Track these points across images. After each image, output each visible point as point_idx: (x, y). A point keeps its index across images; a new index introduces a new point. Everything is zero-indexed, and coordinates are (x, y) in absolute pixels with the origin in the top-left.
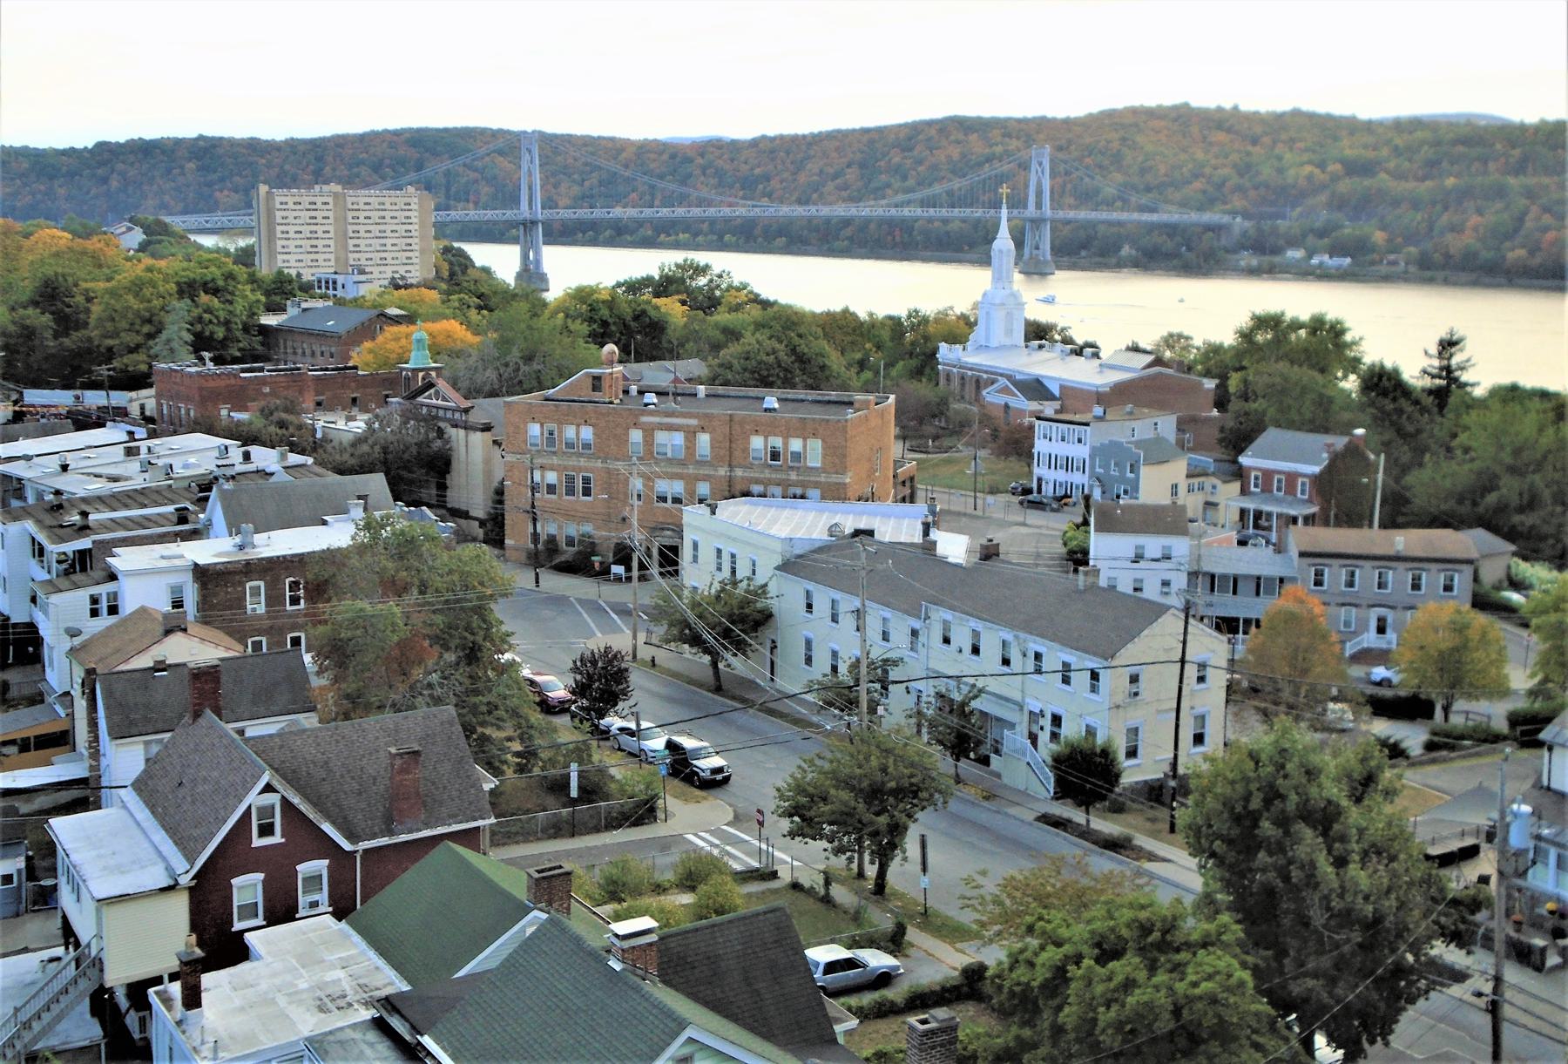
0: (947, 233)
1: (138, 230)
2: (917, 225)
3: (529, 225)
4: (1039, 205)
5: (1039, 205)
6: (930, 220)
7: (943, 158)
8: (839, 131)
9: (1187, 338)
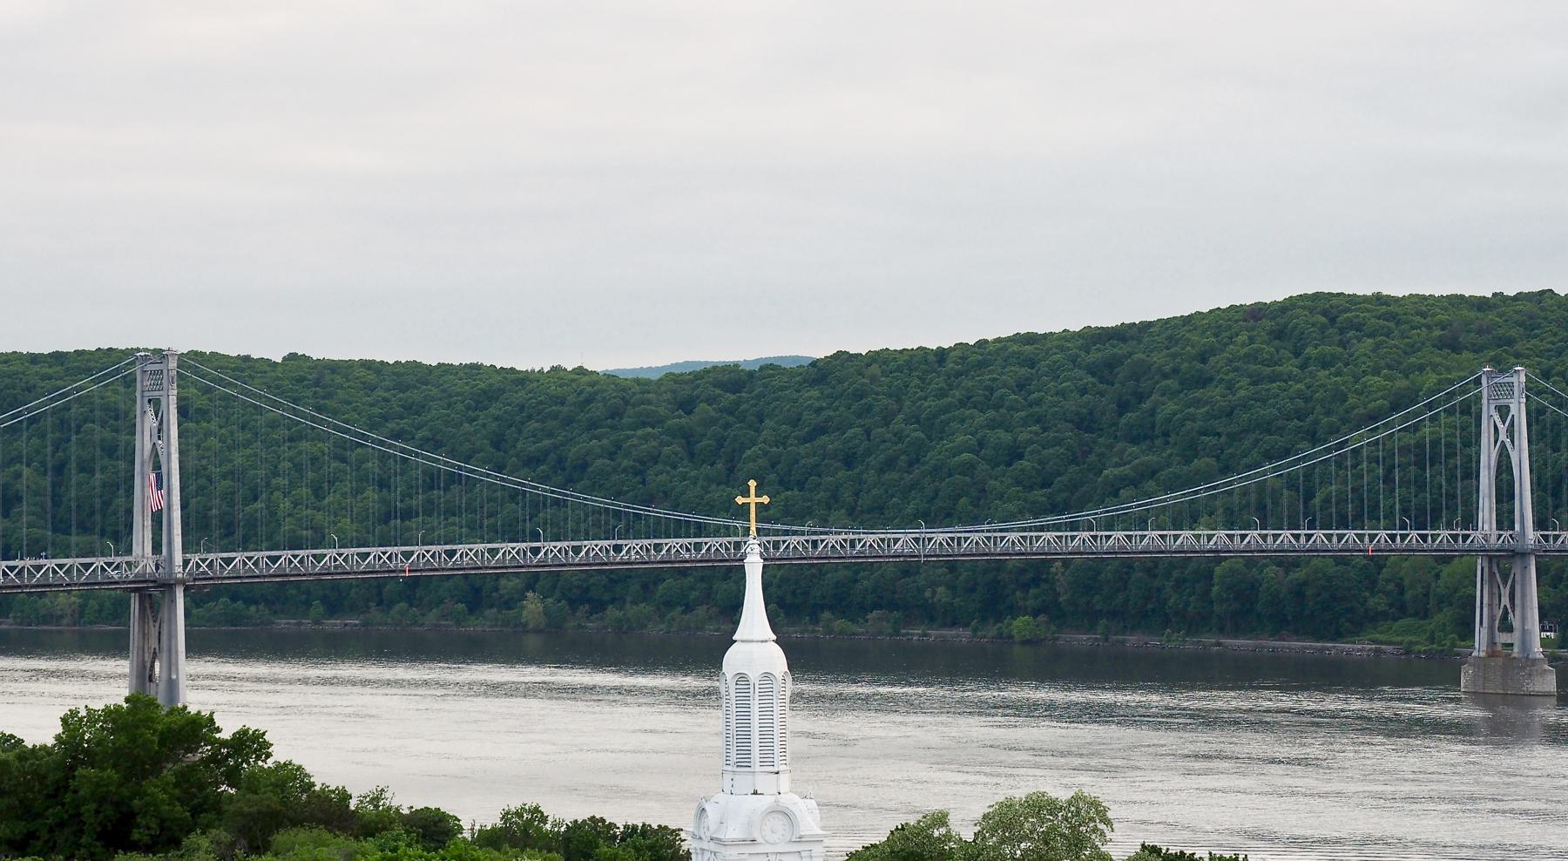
4: (1505, 519)
5: (1505, 519)
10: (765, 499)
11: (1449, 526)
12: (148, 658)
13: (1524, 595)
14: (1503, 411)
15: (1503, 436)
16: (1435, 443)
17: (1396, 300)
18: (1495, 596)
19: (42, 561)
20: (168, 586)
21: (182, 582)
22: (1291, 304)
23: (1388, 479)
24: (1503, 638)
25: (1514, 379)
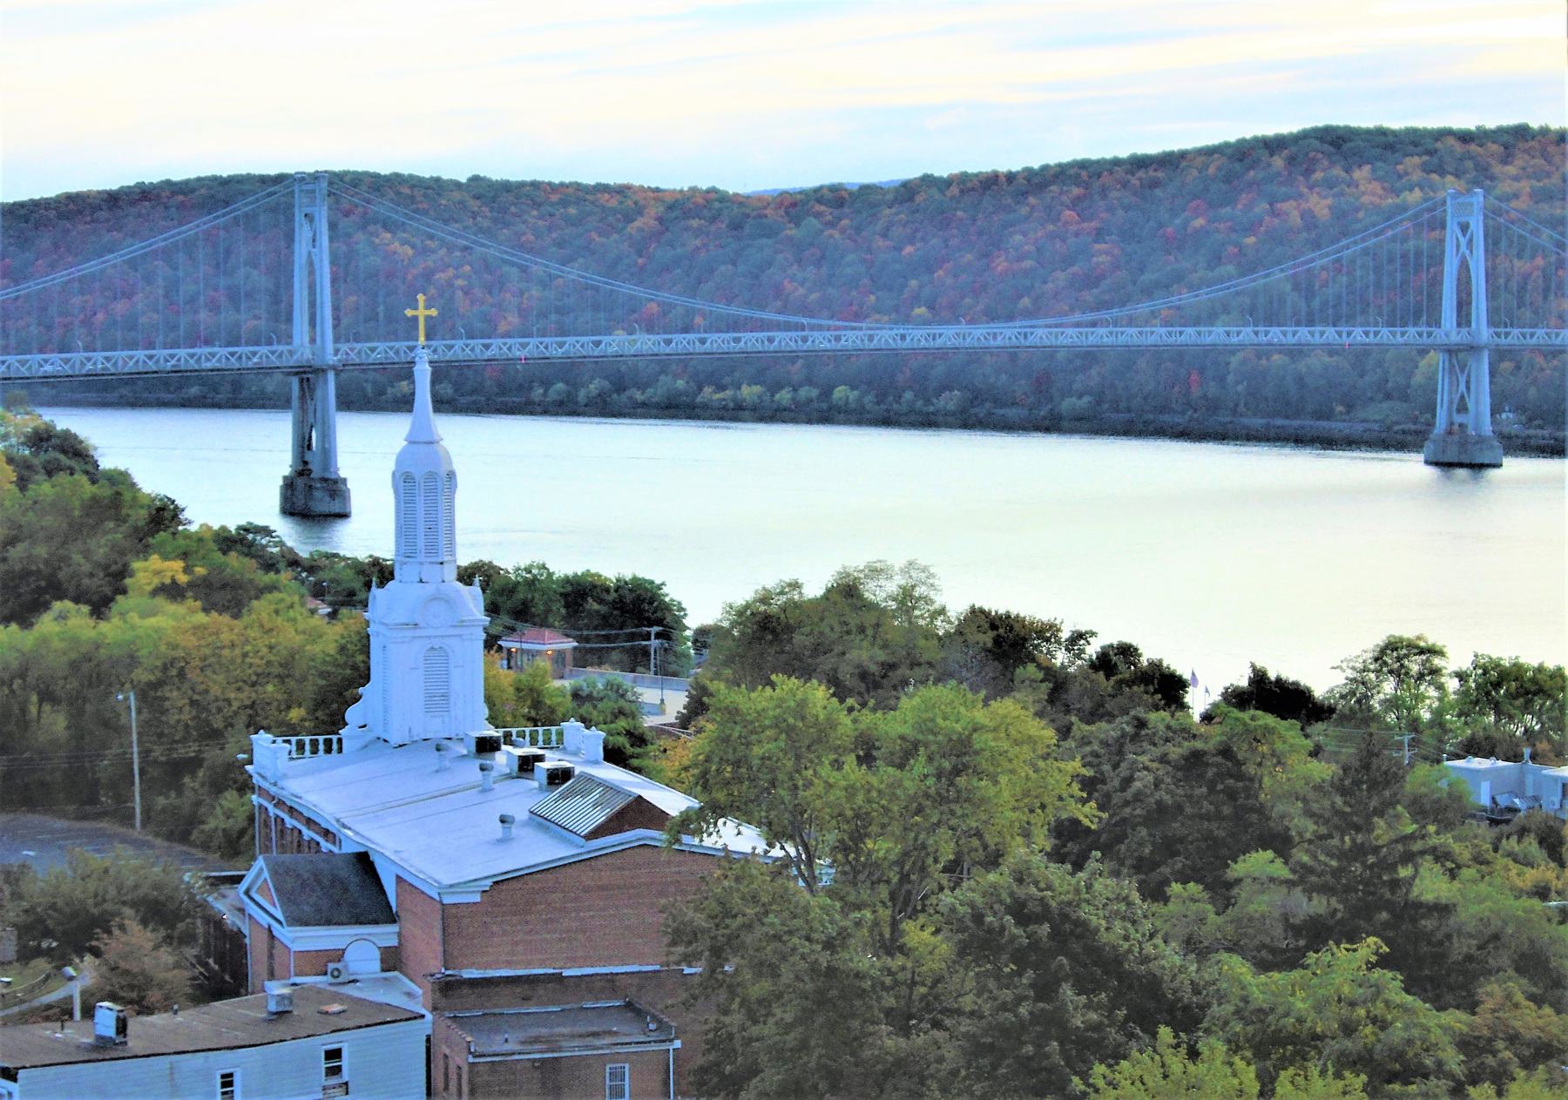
0: (1300, 380)
1: (537, 399)
2: (1235, 361)
3: (308, 376)
4: (1463, 318)
5: (1463, 318)
6: (1263, 351)
7: (1295, 219)
8: (1083, 165)
9: (933, 576)
10: (434, 312)
11: (1415, 325)
12: (307, 430)
13: (1478, 381)
14: (1464, 228)
15: (1463, 248)
16: (1418, 254)
17: (1394, 133)
18: (1454, 383)
19: (216, 349)
20: (320, 371)
21: (334, 368)
22: (1305, 135)
23: (1378, 284)
24: (1458, 419)
25: (1474, 200)
